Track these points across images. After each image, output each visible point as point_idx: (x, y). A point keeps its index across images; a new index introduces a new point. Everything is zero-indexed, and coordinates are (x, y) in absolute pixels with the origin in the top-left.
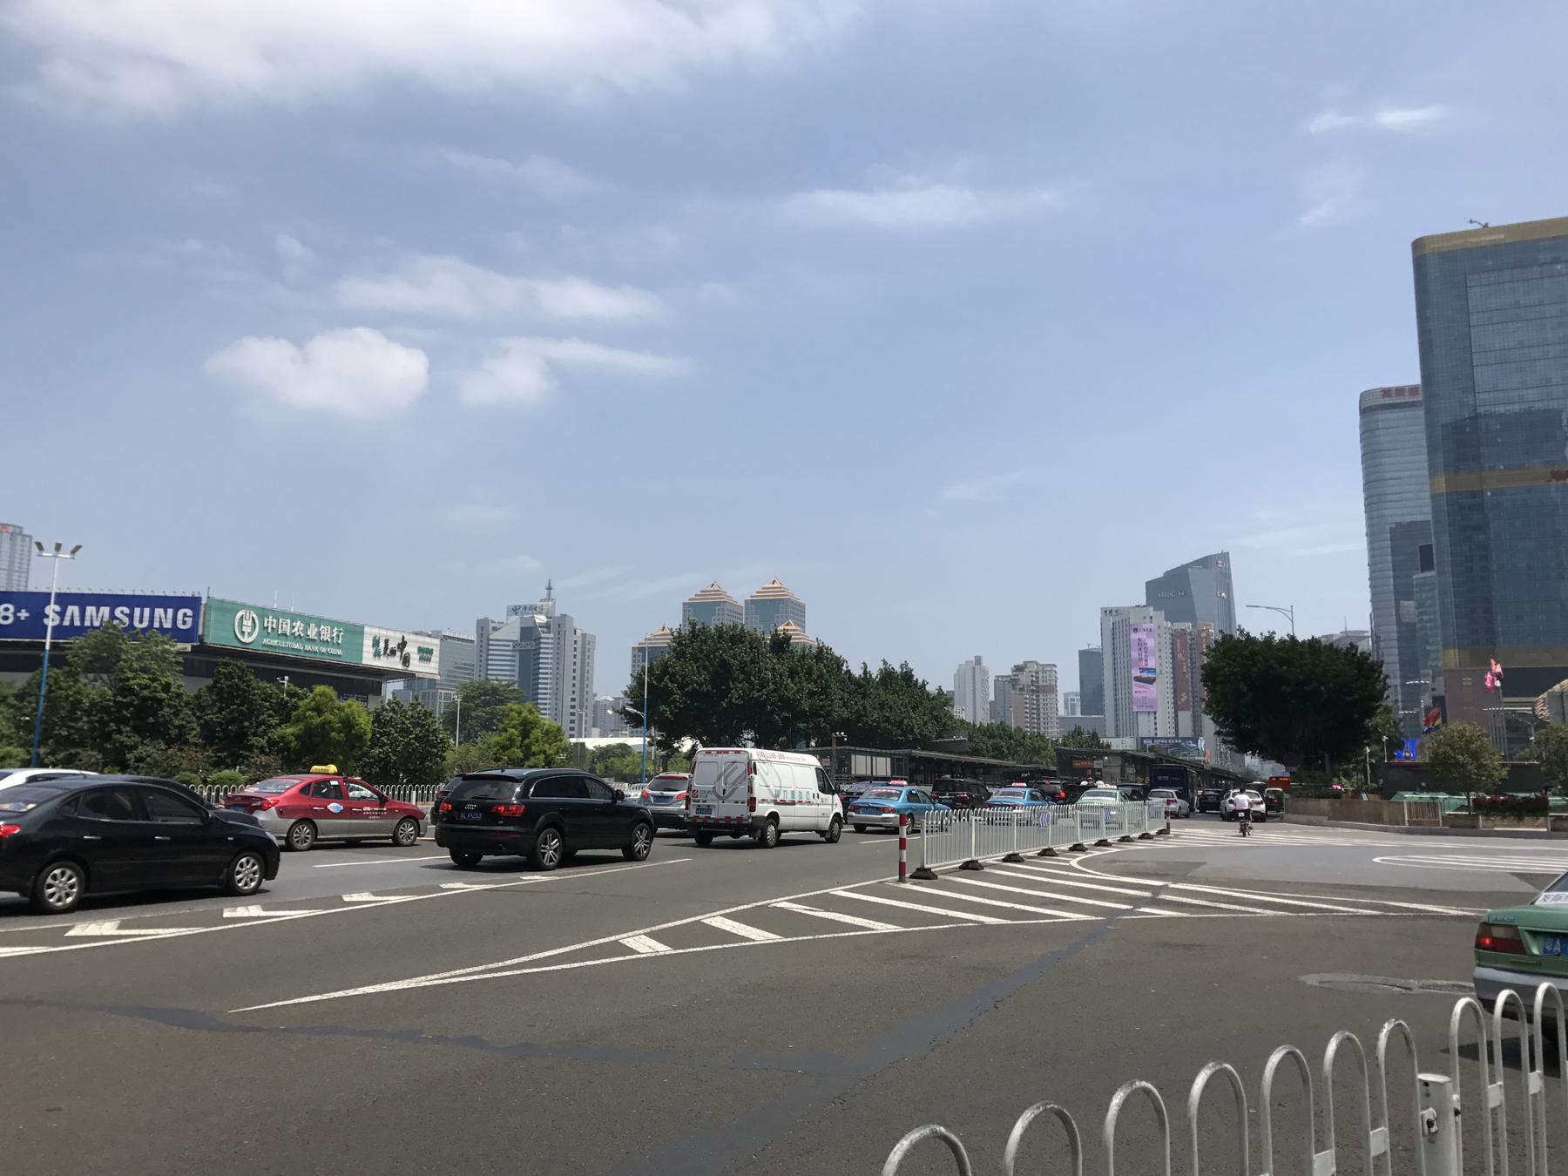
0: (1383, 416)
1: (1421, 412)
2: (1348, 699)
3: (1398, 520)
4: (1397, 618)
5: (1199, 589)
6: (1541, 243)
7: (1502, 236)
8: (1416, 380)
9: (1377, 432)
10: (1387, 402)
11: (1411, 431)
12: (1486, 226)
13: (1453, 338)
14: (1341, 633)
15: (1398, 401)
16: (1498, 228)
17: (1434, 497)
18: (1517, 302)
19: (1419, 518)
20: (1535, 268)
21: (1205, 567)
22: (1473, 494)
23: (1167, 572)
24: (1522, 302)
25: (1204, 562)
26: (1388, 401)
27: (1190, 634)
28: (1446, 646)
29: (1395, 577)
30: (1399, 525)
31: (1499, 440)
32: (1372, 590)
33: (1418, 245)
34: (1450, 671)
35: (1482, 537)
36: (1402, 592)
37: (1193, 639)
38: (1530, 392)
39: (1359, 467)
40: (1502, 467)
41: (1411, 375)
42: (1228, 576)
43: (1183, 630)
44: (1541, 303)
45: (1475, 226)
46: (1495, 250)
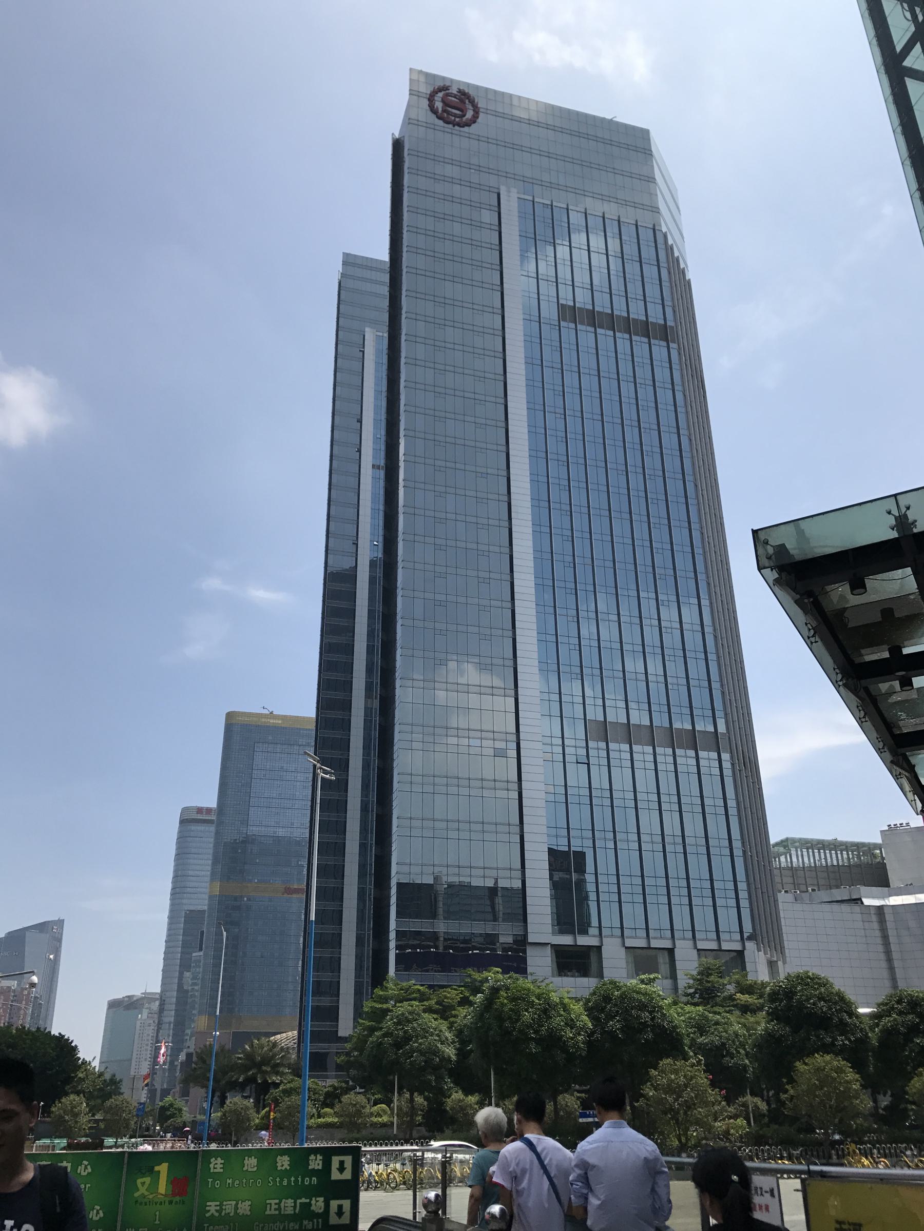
0: (194, 827)
1: (212, 828)
2: (50, 1072)
3: (192, 908)
4: (178, 986)
5: (33, 949)
6: (302, 731)
7: (280, 722)
8: (213, 803)
9: (189, 839)
10: (199, 818)
11: (206, 839)
12: (272, 713)
13: (240, 784)
14: (142, 994)
15: (207, 818)
16: (279, 716)
17: (211, 897)
18: (282, 768)
19: (199, 908)
20: (295, 747)
21: (41, 931)
22: (236, 899)
23: (9, 933)
24: (284, 768)
25: (42, 927)
26: (200, 817)
27: (14, 991)
28: (200, 1013)
29: (182, 953)
30: (191, 911)
31: (258, 861)
32: (164, 962)
33: (230, 716)
34: (200, 1033)
35: (237, 930)
36: (185, 965)
37: (16, 996)
38: (281, 830)
39: (172, 864)
40: (256, 881)
41: (211, 802)
42: (60, 940)
43: (8, 987)
44: (296, 771)
45: (266, 712)
46: (275, 729)
